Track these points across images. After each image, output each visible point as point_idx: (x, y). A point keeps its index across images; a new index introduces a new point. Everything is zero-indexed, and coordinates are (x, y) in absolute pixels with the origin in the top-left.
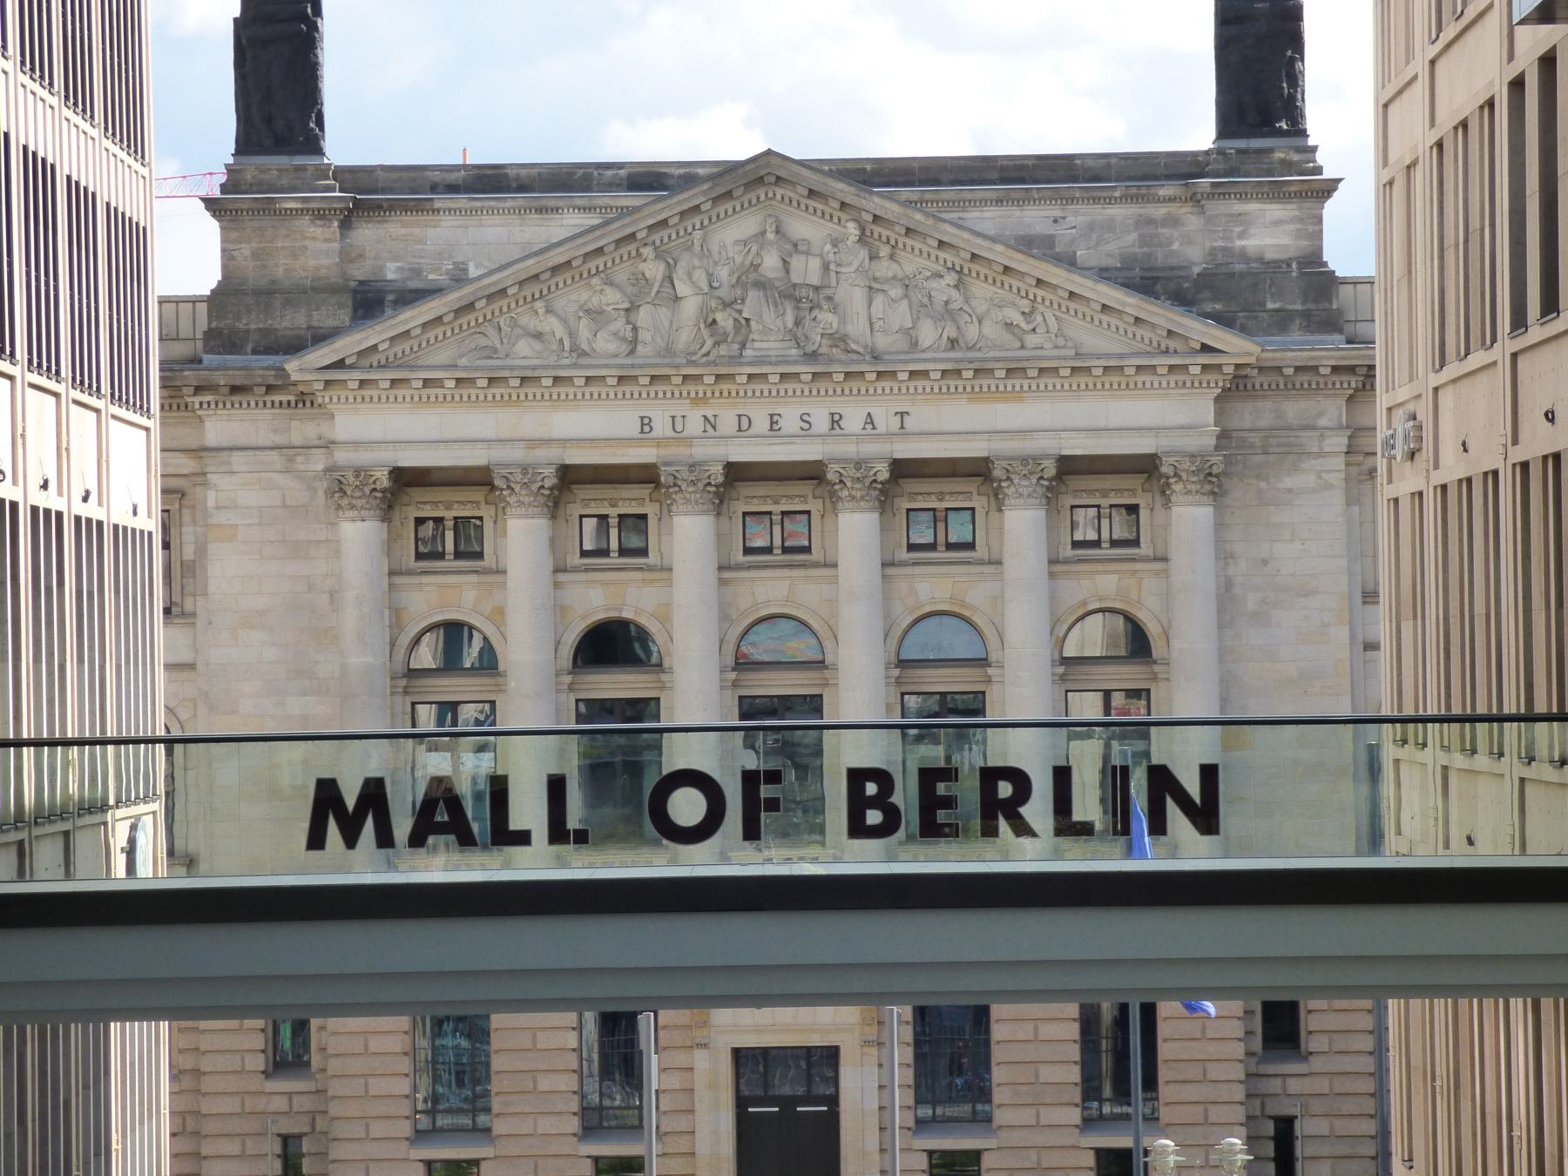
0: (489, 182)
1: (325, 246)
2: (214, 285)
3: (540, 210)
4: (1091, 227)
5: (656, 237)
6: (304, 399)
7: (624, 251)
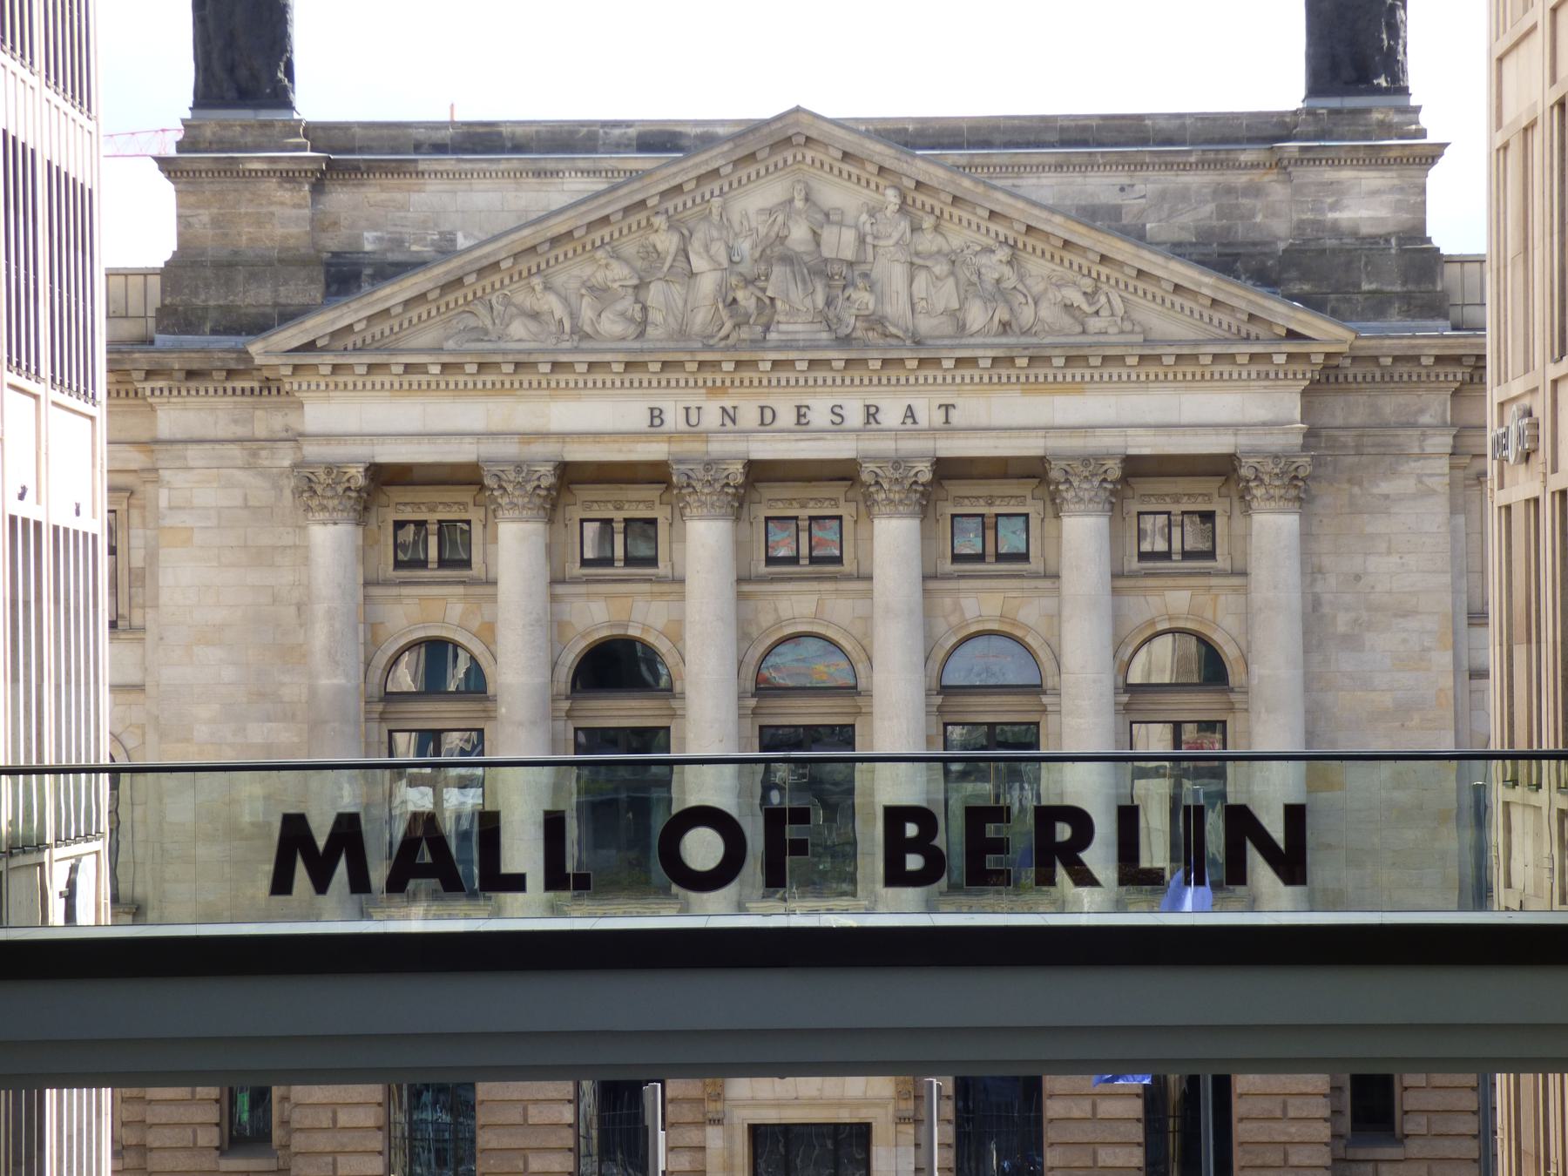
0: (480, 141)
1: (295, 212)
2: (168, 256)
3: (538, 174)
5: (670, 205)
6: (270, 386)
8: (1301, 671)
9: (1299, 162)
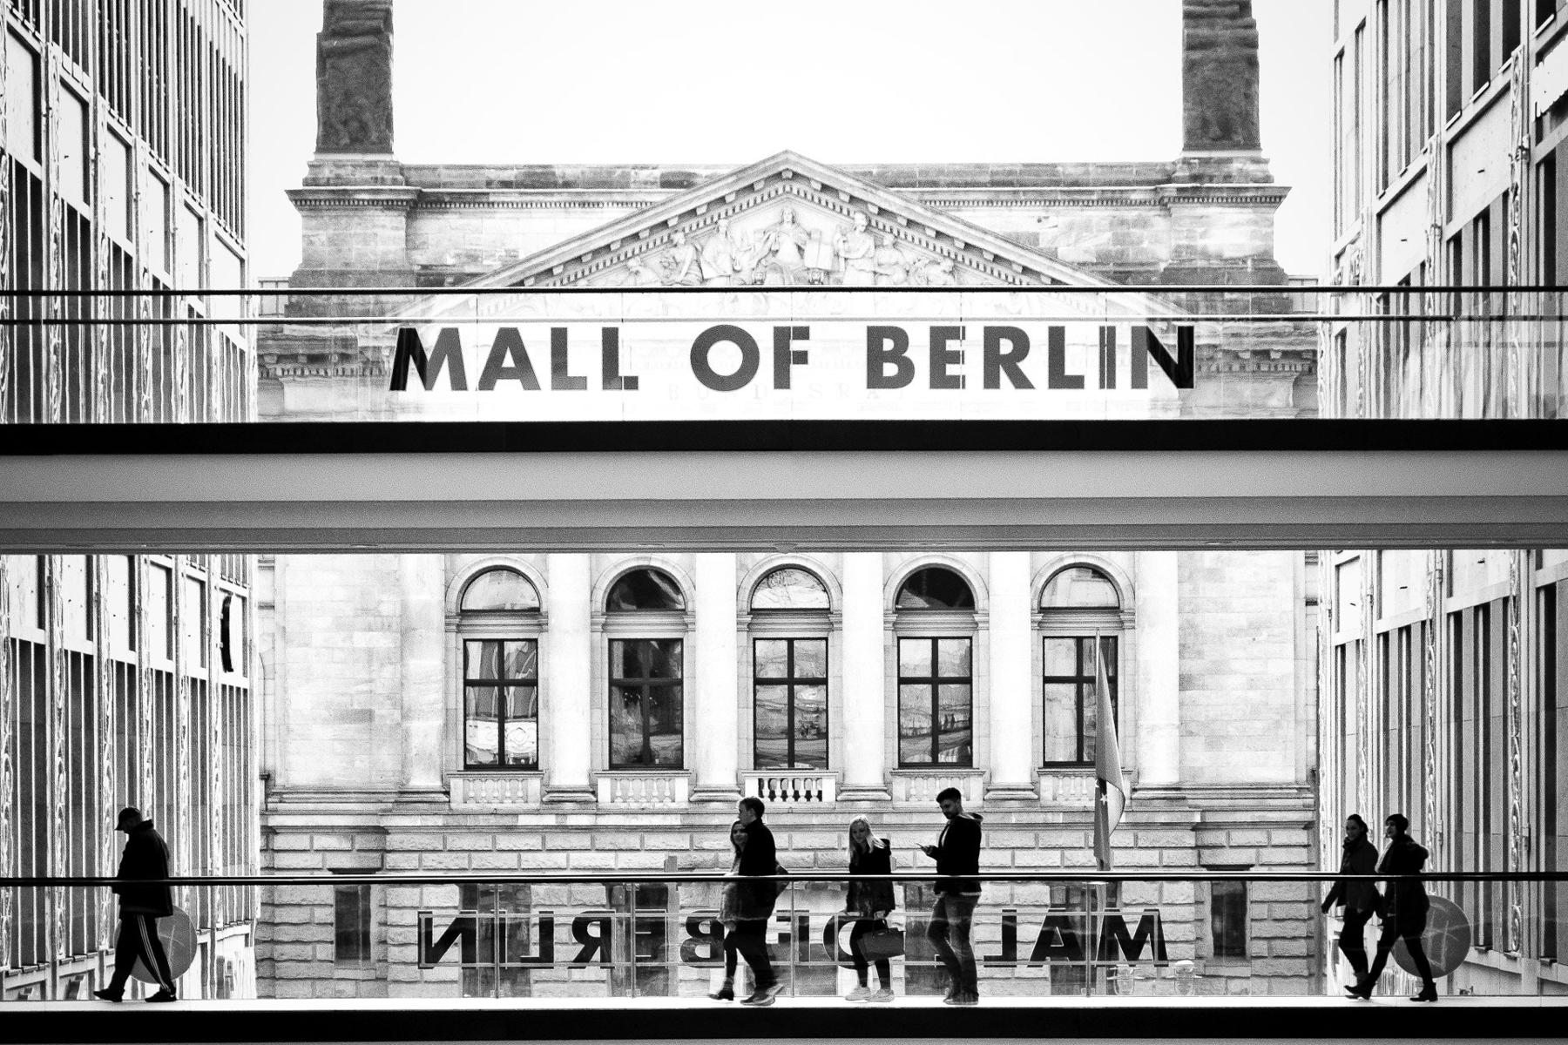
0: (538, 181)
1: (393, 233)
2: (295, 268)
3: (583, 204)
5: (686, 225)
7: (657, 237)
9: (1177, 200)
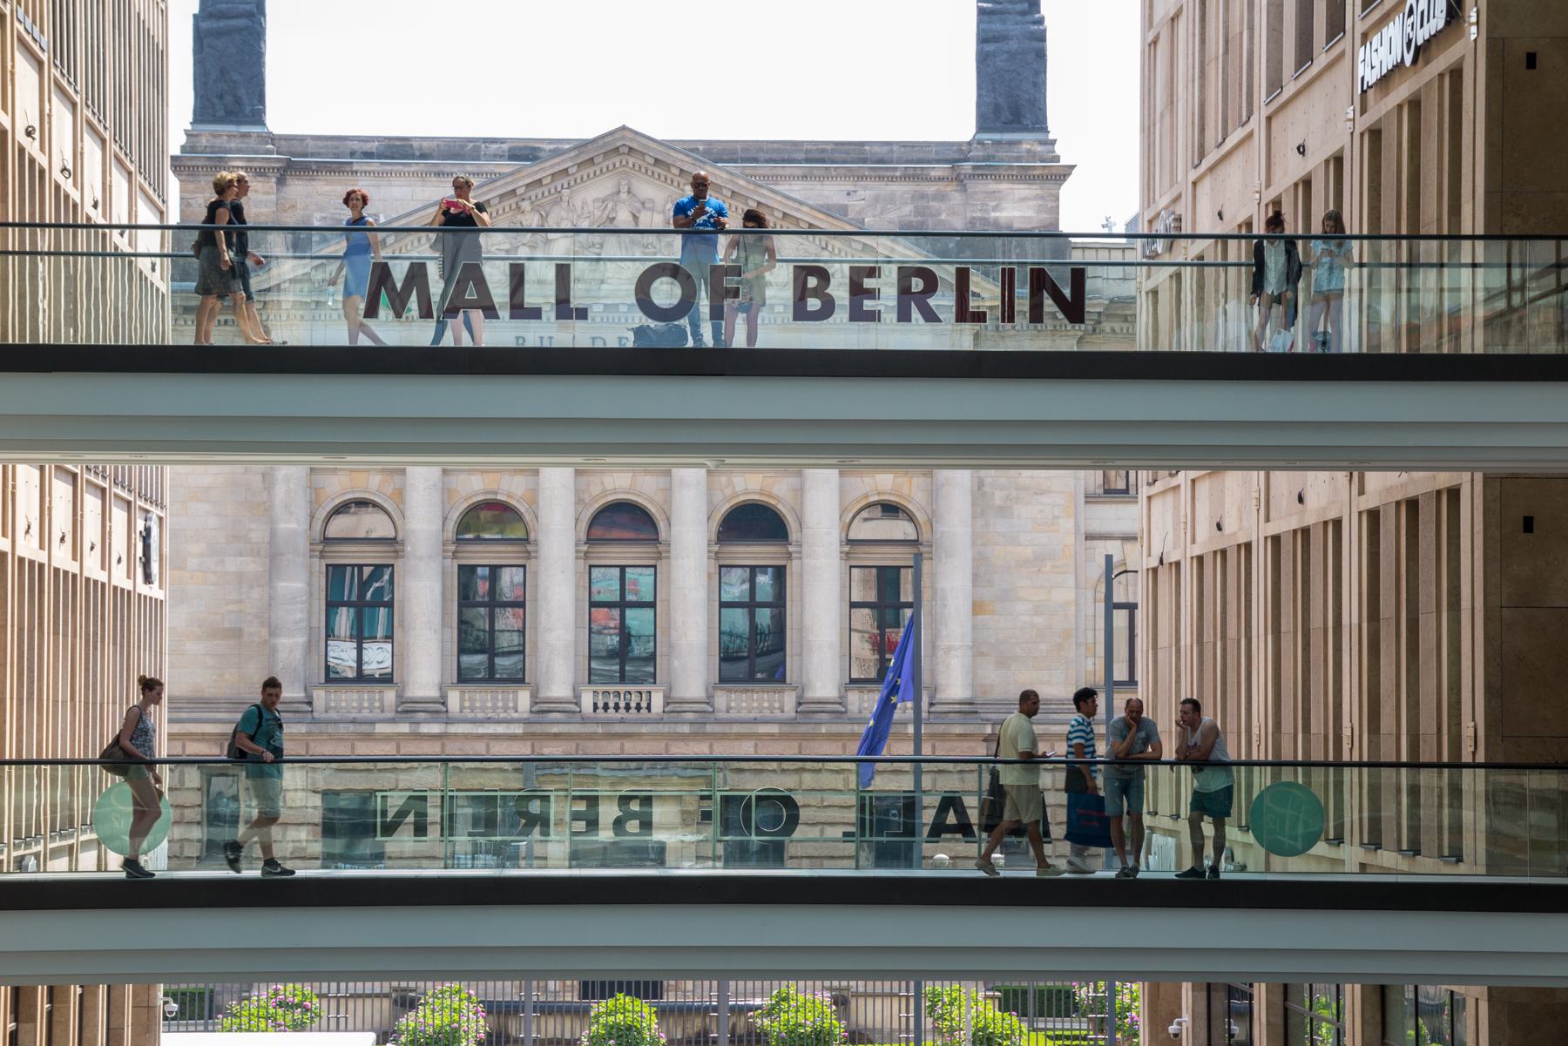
1: (265, 197)
4: (876, 199)
5: (532, 194)
8: (969, 529)
9: (972, 177)
